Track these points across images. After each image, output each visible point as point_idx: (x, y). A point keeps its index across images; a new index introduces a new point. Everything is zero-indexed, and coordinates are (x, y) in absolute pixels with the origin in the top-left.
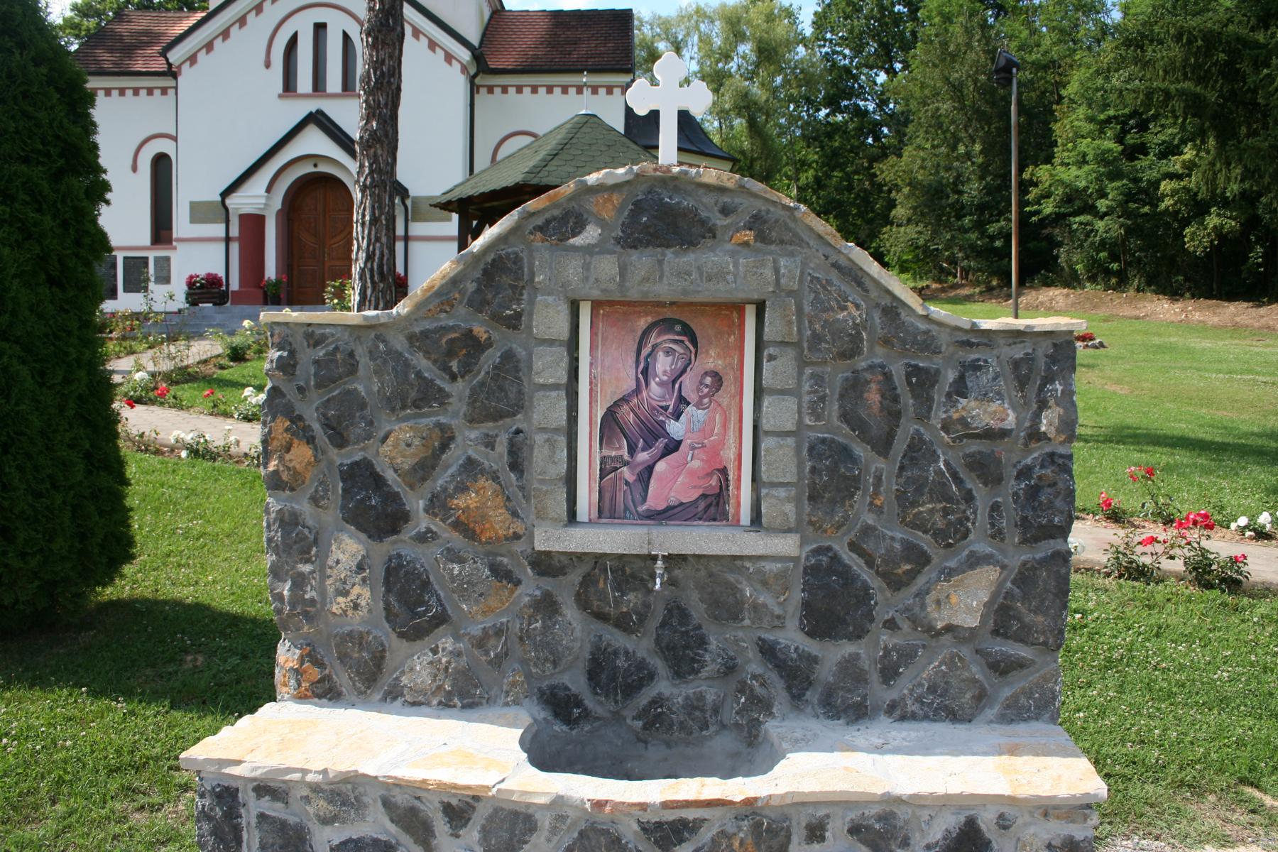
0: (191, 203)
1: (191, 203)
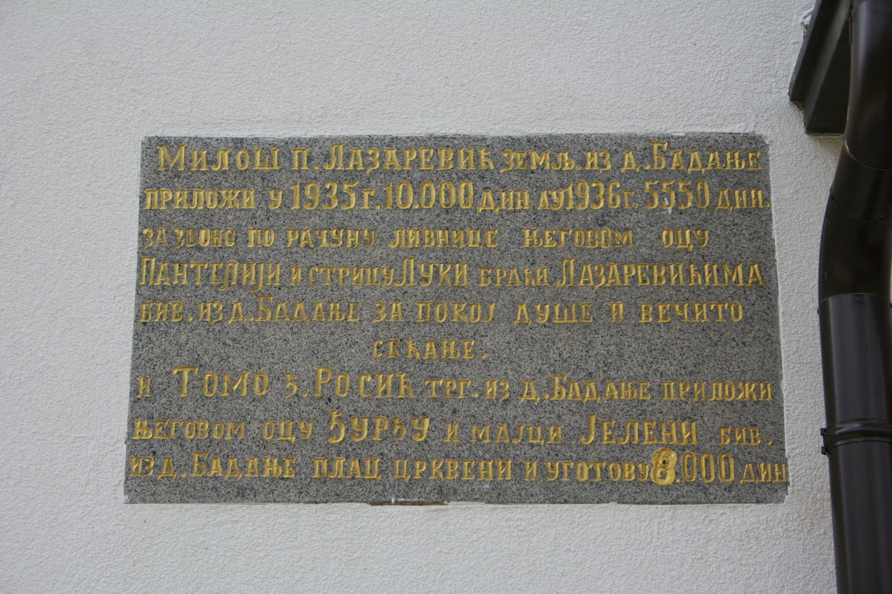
0: (168, 165)
1: (168, 165)
